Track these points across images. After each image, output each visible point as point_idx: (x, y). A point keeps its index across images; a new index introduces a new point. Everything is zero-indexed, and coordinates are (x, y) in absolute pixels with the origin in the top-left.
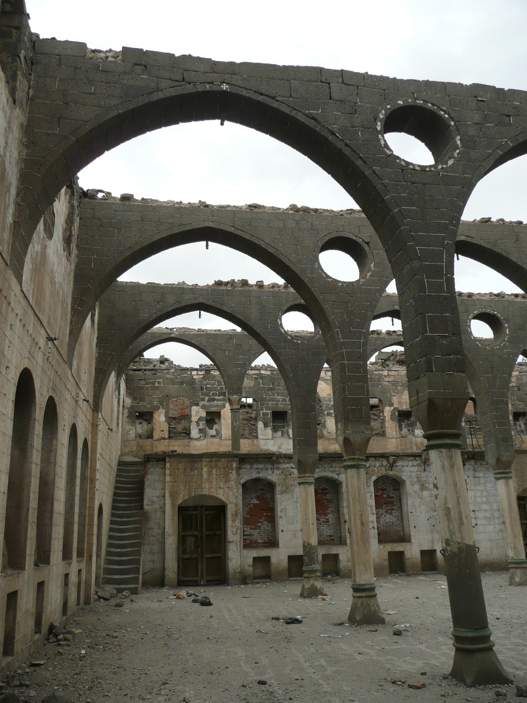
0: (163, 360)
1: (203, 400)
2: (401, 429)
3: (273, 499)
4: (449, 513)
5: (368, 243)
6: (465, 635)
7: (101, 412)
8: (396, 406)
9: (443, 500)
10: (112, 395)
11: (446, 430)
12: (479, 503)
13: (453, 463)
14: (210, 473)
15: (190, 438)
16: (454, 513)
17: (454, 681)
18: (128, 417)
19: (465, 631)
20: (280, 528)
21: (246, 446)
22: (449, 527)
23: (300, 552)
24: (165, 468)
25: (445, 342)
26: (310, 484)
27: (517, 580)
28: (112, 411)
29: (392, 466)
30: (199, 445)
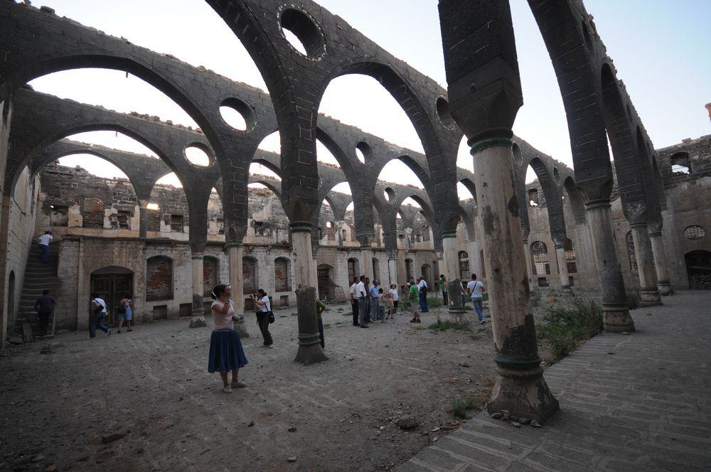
0: (78, 169)
1: (116, 202)
2: (256, 232)
3: (171, 270)
5: (253, 108)
7: (13, 196)
10: (26, 187)
14: (120, 252)
15: (103, 228)
16: (305, 270)
18: (42, 208)
20: (175, 287)
21: (150, 235)
23: (191, 301)
24: (79, 247)
26: (200, 258)
28: (26, 200)
29: (251, 251)
30: (109, 232)
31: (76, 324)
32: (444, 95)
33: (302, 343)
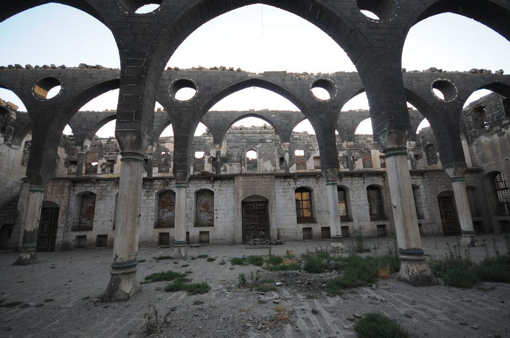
1: (106, 154)
8: (211, 155)
12: (221, 205)
14: (52, 190)
20: (95, 219)
29: (168, 184)
31: (235, 242)
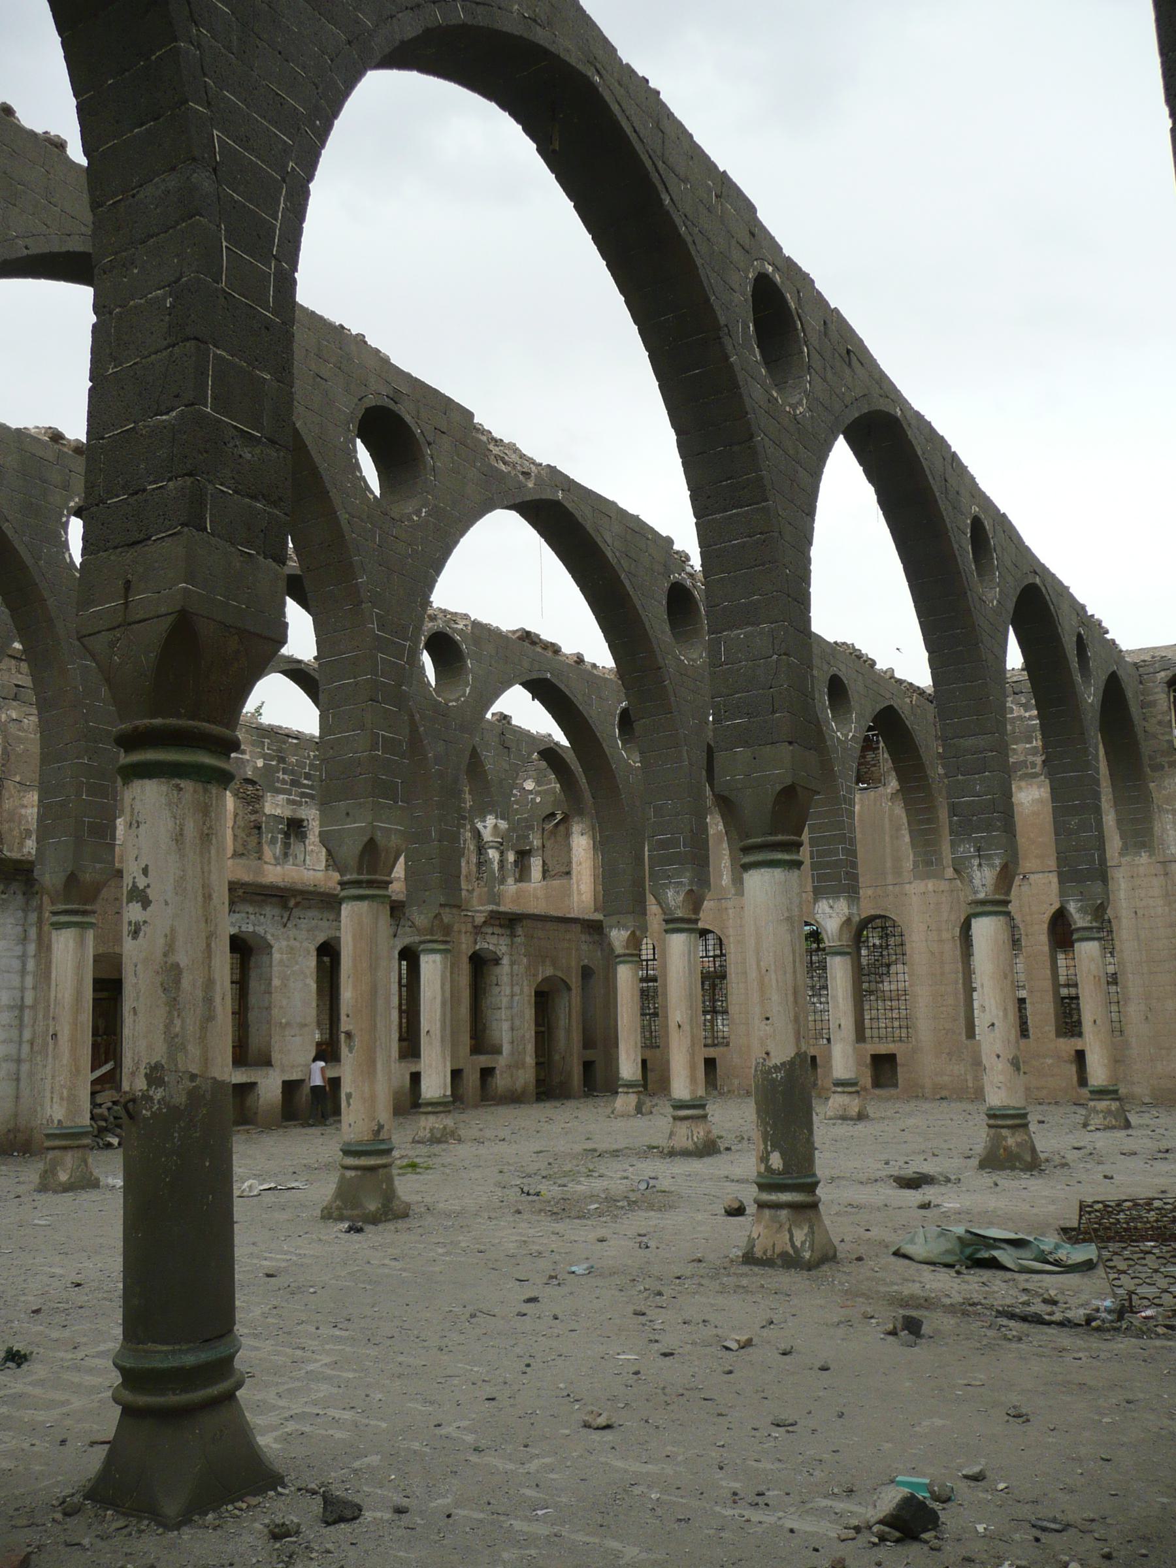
4: (177, 981)
6: (172, 1363)
9: (161, 941)
11: (213, 726)
13: (210, 828)
17: (113, 1521)
19: (173, 1352)
22: (168, 1026)
25: (248, 456)
27: (63, 1177)
32: (776, 268)
33: (128, 1396)
